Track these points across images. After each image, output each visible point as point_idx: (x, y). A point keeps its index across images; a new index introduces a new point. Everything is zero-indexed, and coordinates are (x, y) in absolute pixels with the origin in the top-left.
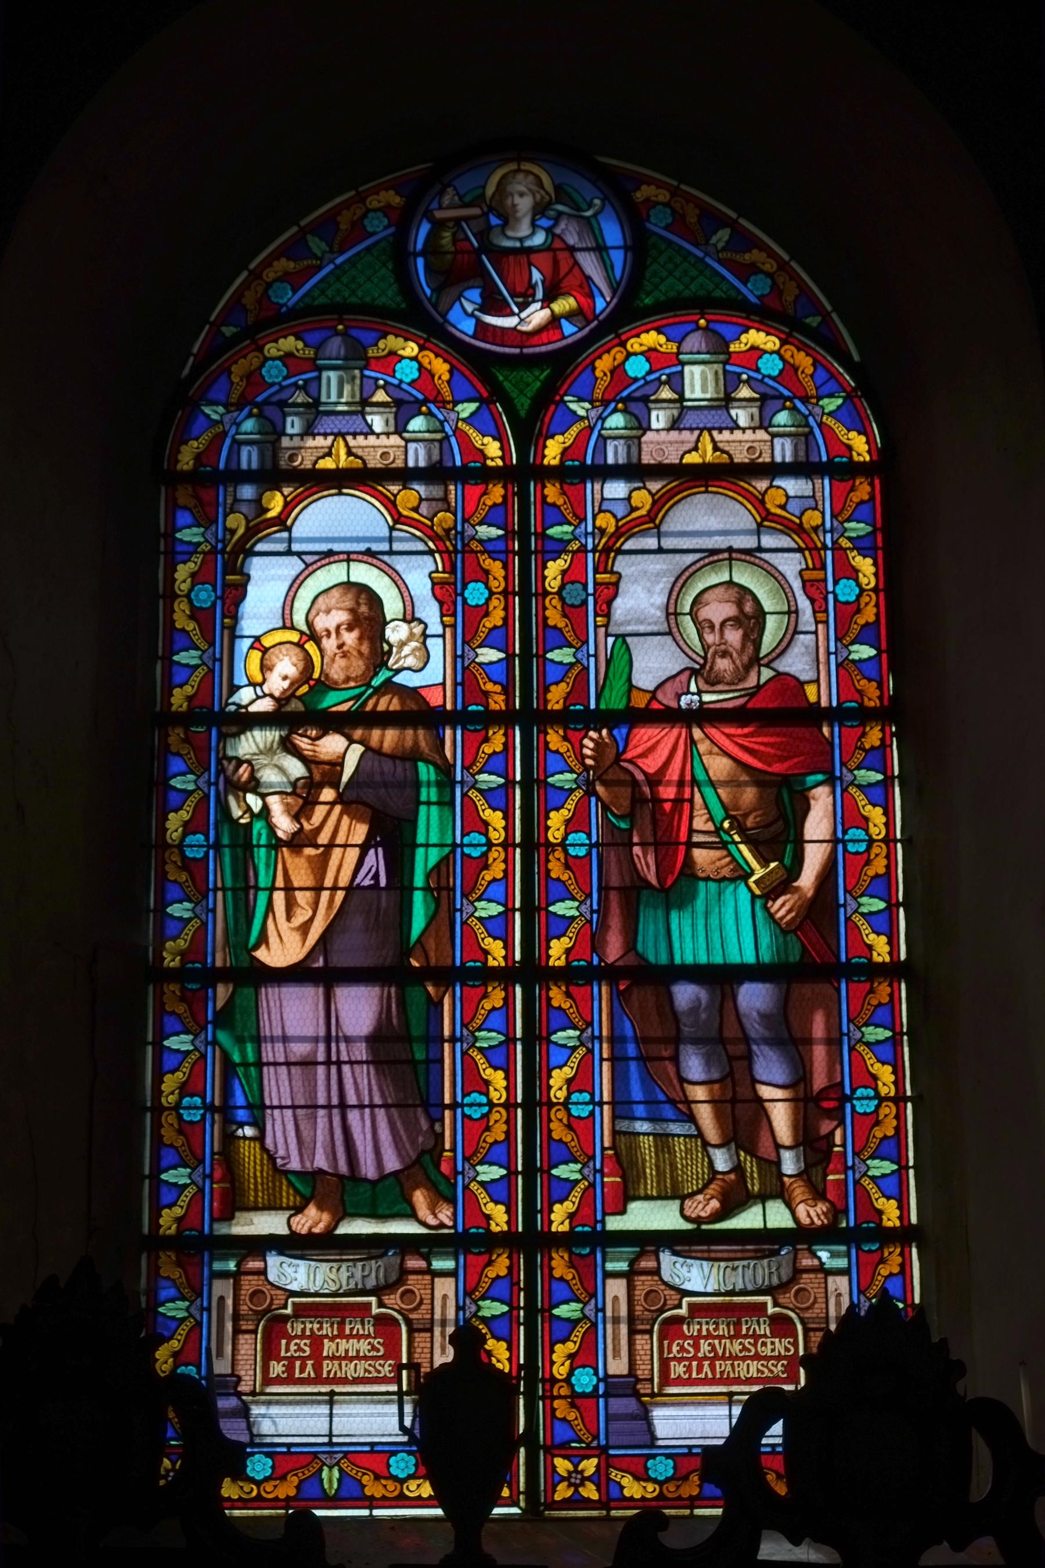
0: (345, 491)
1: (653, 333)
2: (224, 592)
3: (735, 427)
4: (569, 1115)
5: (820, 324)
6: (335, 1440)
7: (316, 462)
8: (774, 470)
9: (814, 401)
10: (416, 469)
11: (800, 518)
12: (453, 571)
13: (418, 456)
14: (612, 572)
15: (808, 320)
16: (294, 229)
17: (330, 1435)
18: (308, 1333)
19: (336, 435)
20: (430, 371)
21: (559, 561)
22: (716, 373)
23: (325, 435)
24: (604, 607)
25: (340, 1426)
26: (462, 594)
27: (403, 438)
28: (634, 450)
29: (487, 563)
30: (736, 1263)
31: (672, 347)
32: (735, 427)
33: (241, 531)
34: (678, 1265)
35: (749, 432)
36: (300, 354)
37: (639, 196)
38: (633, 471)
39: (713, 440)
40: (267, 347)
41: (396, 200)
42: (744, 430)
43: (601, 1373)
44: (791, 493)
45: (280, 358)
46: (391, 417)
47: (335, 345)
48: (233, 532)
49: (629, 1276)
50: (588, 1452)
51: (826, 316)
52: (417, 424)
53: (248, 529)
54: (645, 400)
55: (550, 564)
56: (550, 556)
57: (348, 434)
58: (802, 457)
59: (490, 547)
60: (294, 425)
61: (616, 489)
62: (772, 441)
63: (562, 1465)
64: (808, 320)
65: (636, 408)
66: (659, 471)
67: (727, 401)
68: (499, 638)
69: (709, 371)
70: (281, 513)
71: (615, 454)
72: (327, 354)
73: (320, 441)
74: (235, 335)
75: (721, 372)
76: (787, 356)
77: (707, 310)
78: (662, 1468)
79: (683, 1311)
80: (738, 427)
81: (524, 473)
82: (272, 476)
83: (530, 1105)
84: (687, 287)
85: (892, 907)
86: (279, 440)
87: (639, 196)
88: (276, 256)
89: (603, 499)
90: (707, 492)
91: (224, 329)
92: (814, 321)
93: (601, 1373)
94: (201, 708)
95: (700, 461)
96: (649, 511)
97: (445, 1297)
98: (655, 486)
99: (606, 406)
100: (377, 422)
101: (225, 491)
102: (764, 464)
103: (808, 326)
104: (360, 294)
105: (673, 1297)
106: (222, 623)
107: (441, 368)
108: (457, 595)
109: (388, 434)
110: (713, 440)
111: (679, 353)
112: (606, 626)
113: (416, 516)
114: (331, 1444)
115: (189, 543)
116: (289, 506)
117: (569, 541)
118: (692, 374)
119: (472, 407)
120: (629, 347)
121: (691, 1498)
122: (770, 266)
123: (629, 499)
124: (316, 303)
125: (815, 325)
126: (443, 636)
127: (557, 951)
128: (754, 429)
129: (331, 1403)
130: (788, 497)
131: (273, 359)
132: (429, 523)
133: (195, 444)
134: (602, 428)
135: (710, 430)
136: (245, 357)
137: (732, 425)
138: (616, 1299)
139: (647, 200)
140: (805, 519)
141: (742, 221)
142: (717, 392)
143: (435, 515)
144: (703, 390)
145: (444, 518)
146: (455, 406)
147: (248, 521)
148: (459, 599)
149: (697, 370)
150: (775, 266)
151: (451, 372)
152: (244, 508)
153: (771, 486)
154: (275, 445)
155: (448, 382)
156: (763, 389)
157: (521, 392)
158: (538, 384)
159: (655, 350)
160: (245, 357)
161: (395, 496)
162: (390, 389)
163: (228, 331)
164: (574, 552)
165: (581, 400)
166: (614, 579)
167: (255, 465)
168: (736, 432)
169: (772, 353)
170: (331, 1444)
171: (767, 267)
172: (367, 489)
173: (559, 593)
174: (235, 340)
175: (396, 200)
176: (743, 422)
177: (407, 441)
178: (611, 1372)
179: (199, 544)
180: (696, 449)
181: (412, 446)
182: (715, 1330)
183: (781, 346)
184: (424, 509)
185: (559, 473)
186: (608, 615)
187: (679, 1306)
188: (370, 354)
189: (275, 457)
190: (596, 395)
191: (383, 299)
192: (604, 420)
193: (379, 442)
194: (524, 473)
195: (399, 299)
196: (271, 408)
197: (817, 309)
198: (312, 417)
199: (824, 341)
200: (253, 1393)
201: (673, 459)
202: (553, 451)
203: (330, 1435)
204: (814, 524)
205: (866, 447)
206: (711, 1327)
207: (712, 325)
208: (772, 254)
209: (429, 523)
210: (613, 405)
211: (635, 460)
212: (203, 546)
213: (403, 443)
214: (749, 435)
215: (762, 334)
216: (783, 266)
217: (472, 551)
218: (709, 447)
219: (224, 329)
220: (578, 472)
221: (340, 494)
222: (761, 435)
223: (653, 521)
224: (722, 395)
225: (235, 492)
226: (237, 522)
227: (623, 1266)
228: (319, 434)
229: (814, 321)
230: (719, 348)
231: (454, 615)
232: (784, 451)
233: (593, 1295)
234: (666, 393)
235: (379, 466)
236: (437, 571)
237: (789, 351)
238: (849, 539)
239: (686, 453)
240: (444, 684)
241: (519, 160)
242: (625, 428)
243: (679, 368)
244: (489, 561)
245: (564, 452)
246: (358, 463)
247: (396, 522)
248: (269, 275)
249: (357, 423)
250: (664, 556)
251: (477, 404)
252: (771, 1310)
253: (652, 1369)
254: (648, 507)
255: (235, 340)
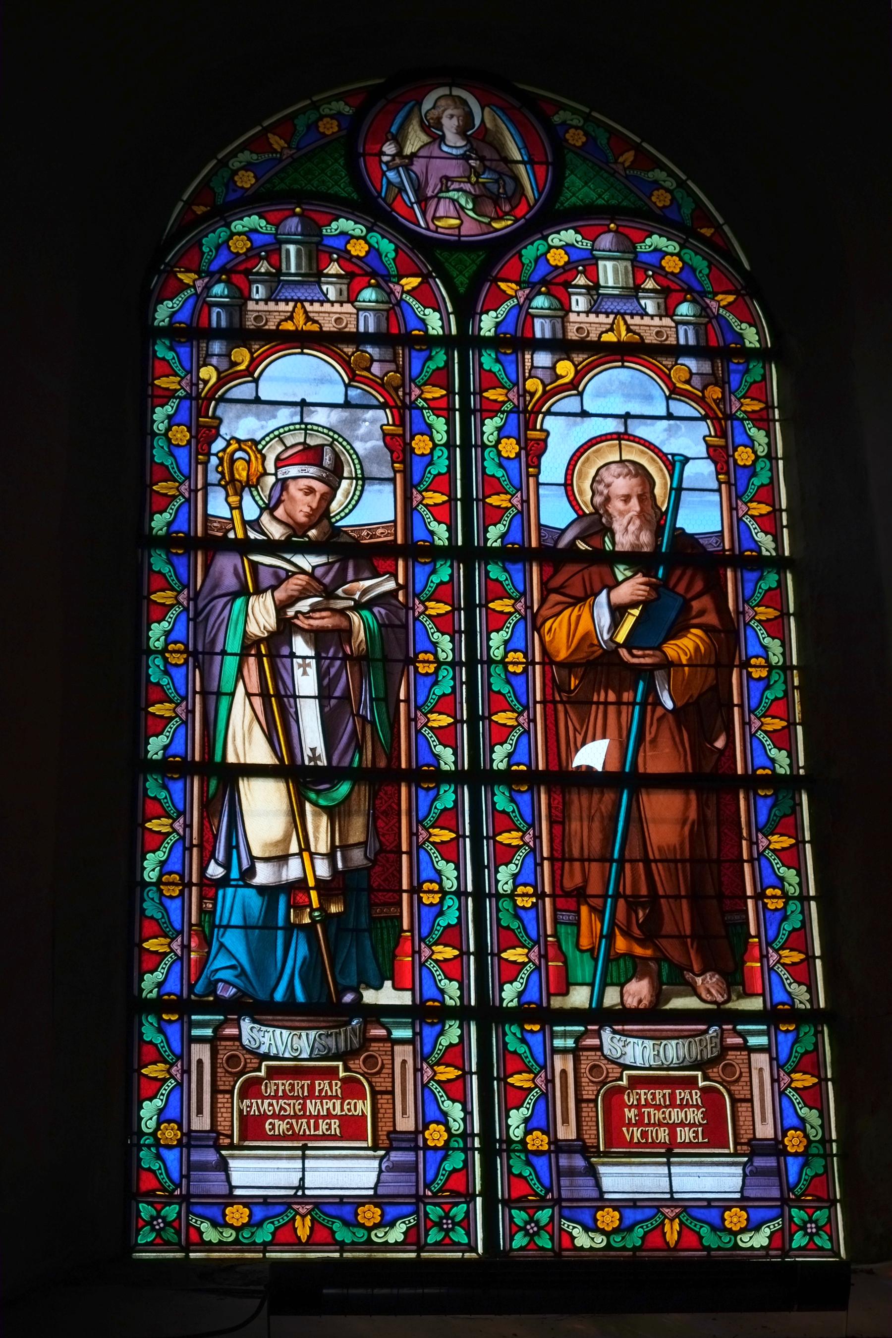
0: (626, 364)
1: (571, 232)
2: (198, 432)
3: (644, 314)
4: (515, 906)
5: (713, 234)
6: (676, 1196)
7: (279, 324)
8: (677, 351)
9: (395, 280)
10: (366, 333)
11: (702, 392)
12: (402, 424)
13: (369, 324)
14: (542, 430)
15: (703, 231)
16: (259, 128)
17: (671, 1192)
18: (280, 1094)
19: (617, 314)
20: (378, 250)
21: (495, 419)
22: (626, 268)
23: (287, 301)
24: (535, 459)
25: (679, 1184)
26: (733, 456)
27: (673, 320)
28: (559, 326)
29: (432, 419)
30: (629, 1040)
31: (587, 244)
32: (644, 314)
33: (214, 380)
34: (255, 1031)
35: (337, 305)
36: (579, 245)
37: (557, 119)
38: (561, 346)
39: (626, 323)
40: (234, 224)
41: (347, 110)
42: (652, 317)
43: (185, 1130)
44: (694, 371)
45: (561, 247)
46: (344, 287)
47: (293, 224)
48: (532, 395)
49: (576, 1052)
50: (422, 1214)
51: (718, 228)
52: (685, 309)
53: (544, 392)
54: (567, 284)
55: (487, 421)
56: (160, 401)
57: (306, 300)
58: (384, 328)
59: (432, 404)
60: (259, 291)
61: (543, 359)
62: (357, 314)
63: (520, 1216)
64: (703, 231)
65: (237, 279)
66: (583, 346)
67: (634, 291)
68: (444, 483)
69: (621, 265)
70: (573, 380)
71: (541, 329)
72: (602, 247)
73: (282, 306)
74: (204, 213)
75: (630, 268)
76: (687, 258)
77: (630, 215)
78: (608, 1218)
79: (262, 1074)
80: (647, 314)
81: (465, 342)
82: (239, 334)
83: (479, 895)
84: (600, 196)
85: (791, 725)
86: (245, 304)
87: (557, 119)
88: (241, 148)
89: (533, 367)
90: (623, 366)
91: (195, 208)
92: (707, 232)
93: (185, 1130)
94: (513, 544)
95: (615, 340)
96: (248, 367)
97: (404, 1062)
98: (578, 358)
99: (532, 288)
100: (650, 306)
101: (198, 347)
102: (350, 333)
103: (703, 235)
104: (315, 183)
105: (615, 1071)
106: (528, 472)
107: (387, 247)
108: (729, 456)
109: (342, 303)
110: (626, 323)
111: (593, 249)
112: (537, 476)
113: (687, 387)
114: (672, 1199)
115: (167, 389)
116: (580, 375)
117: (504, 403)
118: (605, 266)
119: (731, 298)
120: (232, 227)
121: (265, 1244)
122: (670, 184)
123: (553, 368)
124: (277, 188)
125: (708, 235)
126: (719, 490)
127: (500, 757)
128: (661, 317)
129: (304, 1158)
130: (691, 374)
131: (557, 248)
132: (700, 394)
133: (170, 304)
134: (529, 307)
135: (623, 315)
136: (214, 232)
137: (641, 311)
138: (200, 1062)
139: (564, 123)
140: (706, 393)
141: (645, 145)
142: (311, 269)
143: (386, 374)
144: (606, 279)
145: (715, 393)
146: (400, 280)
147: (545, 386)
148: (731, 460)
149: (609, 265)
150: (675, 185)
151: (396, 251)
152: (214, 360)
153: (676, 364)
154: (242, 309)
155: (394, 260)
156: (666, 283)
157: (461, 272)
158: (474, 267)
159: (573, 245)
160: (214, 232)
161: (350, 357)
162: (341, 261)
163: (200, 210)
164: (508, 412)
165: (188, 271)
166: (542, 435)
167: (548, 335)
168: (645, 318)
169: (672, 255)
170: (672, 1199)
171: (667, 184)
172: (323, 349)
173: (496, 446)
174: (205, 217)
175: (347, 110)
176: (332, 294)
177: (359, 310)
178: (194, 1127)
179: (176, 391)
180: (611, 330)
181: (682, 329)
182: (653, 1100)
183: (681, 249)
184: (696, 381)
185: (496, 343)
186: (538, 466)
187: (259, 1069)
188: (324, 232)
189: (564, 329)
190: (523, 278)
191: (336, 189)
192: (531, 300)
193: (331, 311)
194: (465, 342)
195: (350, 189)
196: (238, 276)
197: (710, 221)
198: (274, 284)
199: (718, 249)
200: (231, 1147)
201: (593, 337)
202: (487, 324)
203: (671, 1192)
204: (395, 384)
205: (440, 323)
206: (650, 1097)
207: (620, 229)
208: (671, 174)
209: (700, 394)
210: (217, 276)
211: (560, 335)
212: (179, 393)
213: (355, 311)
214: (337, 307)
215: (351, 223)
216: (681, 184)
217: (417, 408)
218: (623, 329)
219: (195, 208)
220: (516, 342)
221: (302, 353)
222: (667, 321)
223: (576, 388)
224: (315, 271)
225: (207, 347)
226: (208, 373)
227: (407, 1033)
228: (281, 300)
229: (707, 232)
230: (627, 249)
231: (727, 473)
232: (687, 336)
233: (544, 1067)
234: (581, 280)
235: (575, 338)
236: (710, 436)
237: (688, 255)
238: (745, 412)
239: (603, 332)
240: (395, 521)
241: (451, 86)
242: (549, 309)
243: (594, 261)
244: (433, 417)
245: (498, 325)
246: (315, 328)
247: (671, 392)
248: (235, 164)
249: (315, 294)
250: (262, 406)
251: (419, 280)
252: (701, 1084)
253: (232, 1125)
254: (246, 363)
255: (205, 217)
